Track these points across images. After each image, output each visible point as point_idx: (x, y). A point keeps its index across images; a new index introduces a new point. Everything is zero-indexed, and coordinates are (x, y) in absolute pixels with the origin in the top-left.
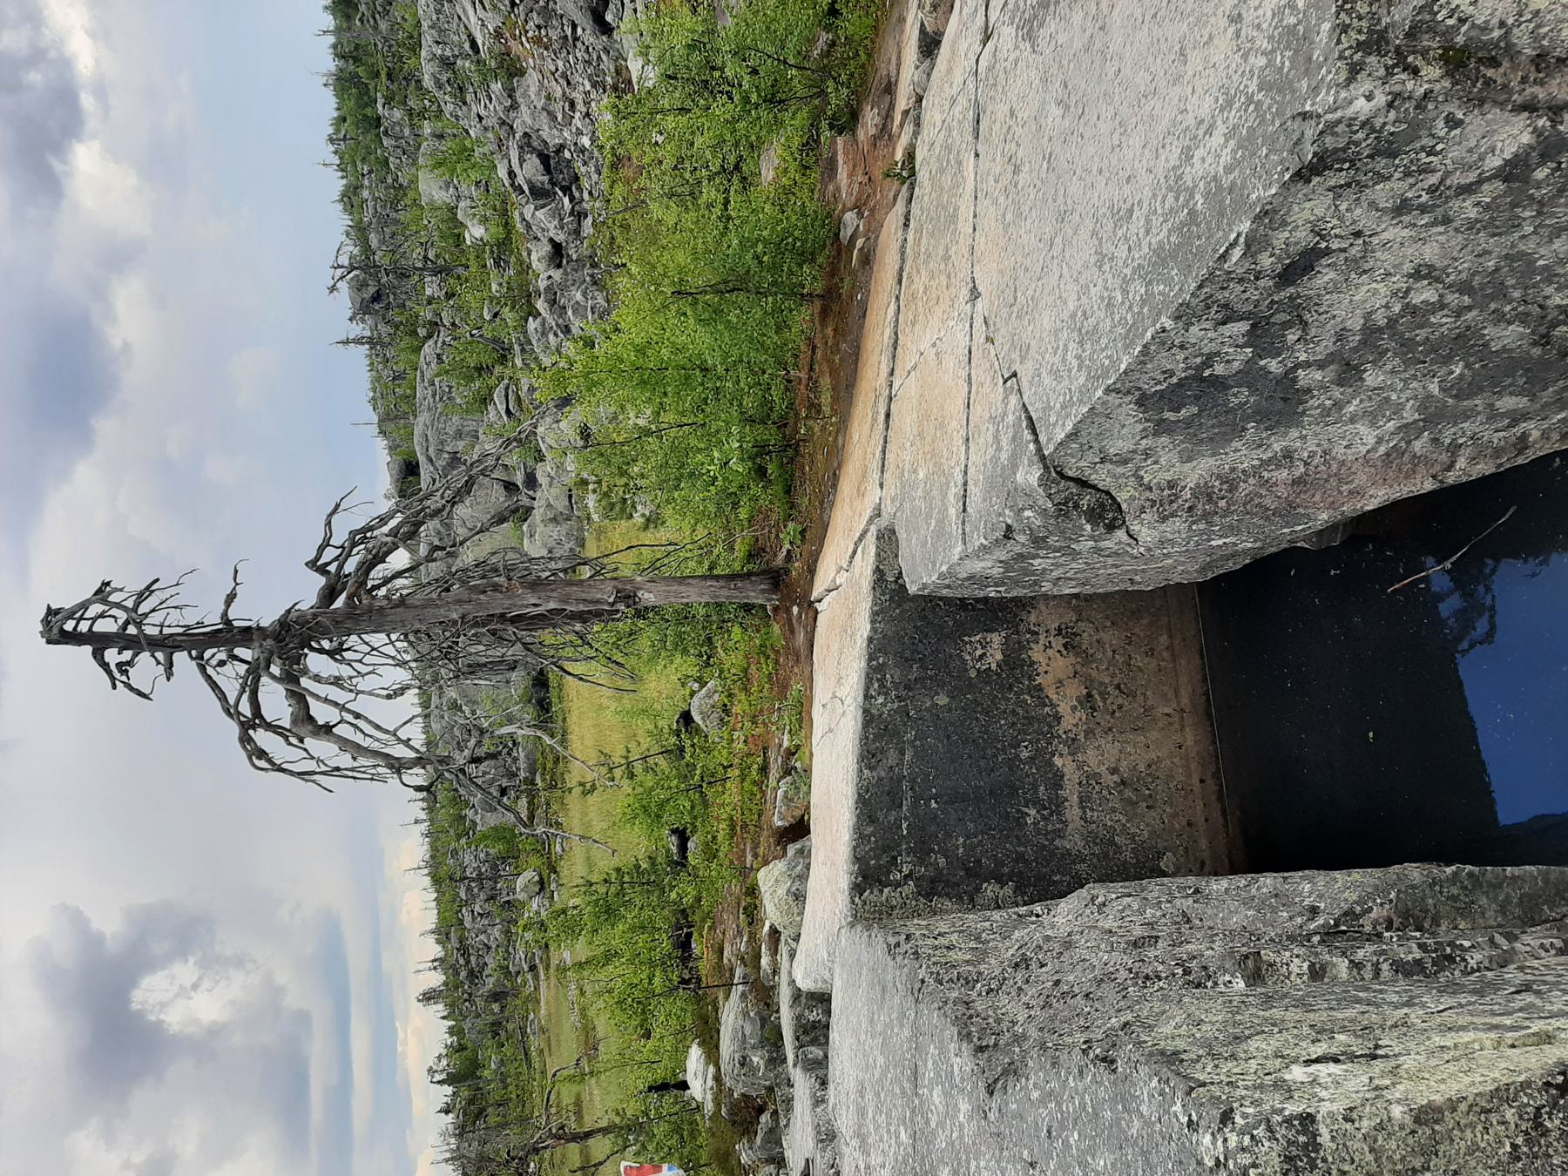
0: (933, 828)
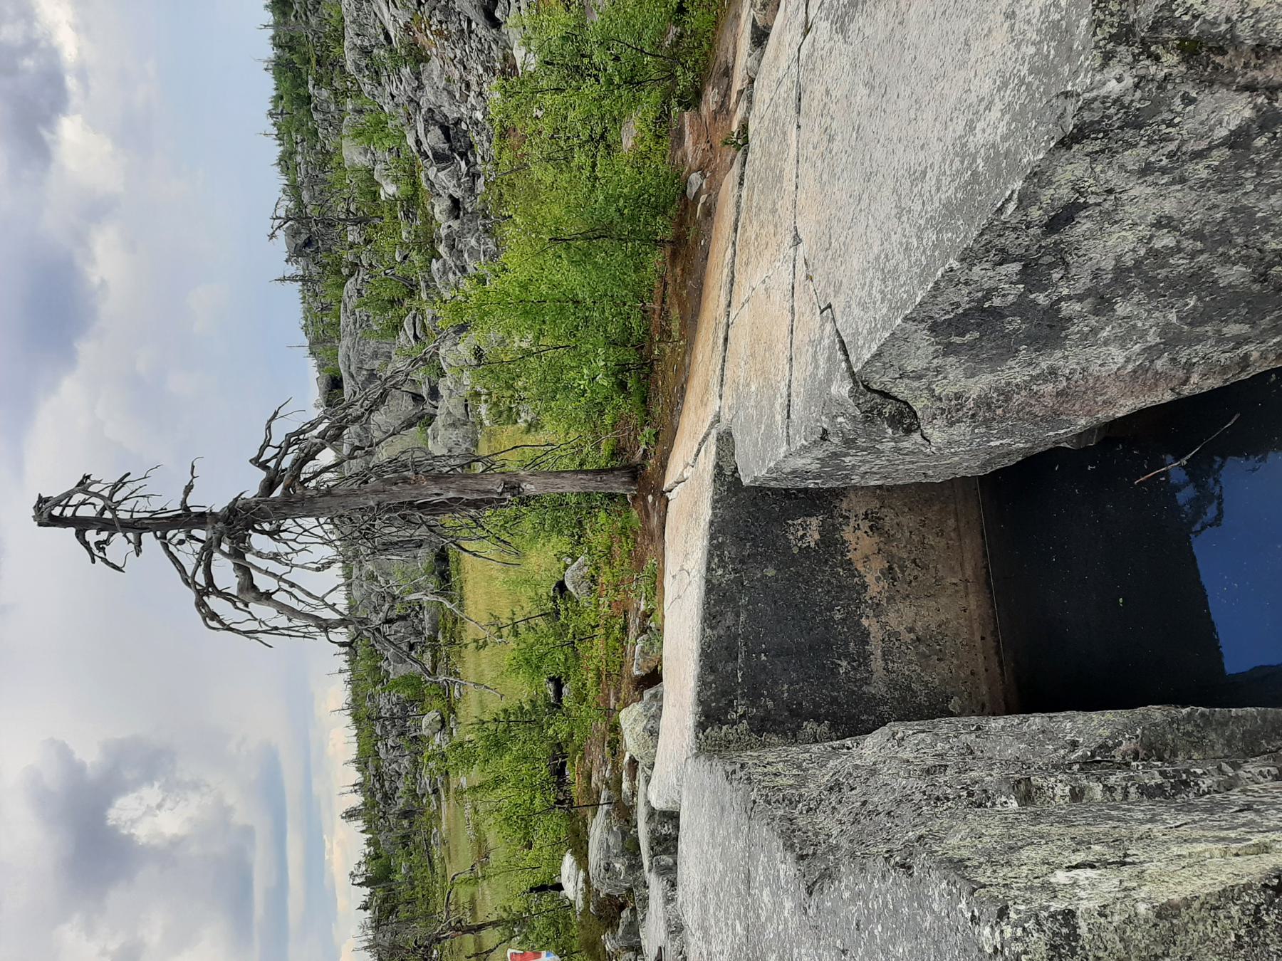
0: (763, 677)
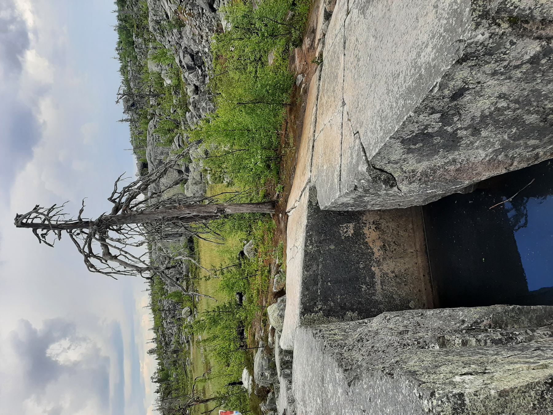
0: (329, 292)
